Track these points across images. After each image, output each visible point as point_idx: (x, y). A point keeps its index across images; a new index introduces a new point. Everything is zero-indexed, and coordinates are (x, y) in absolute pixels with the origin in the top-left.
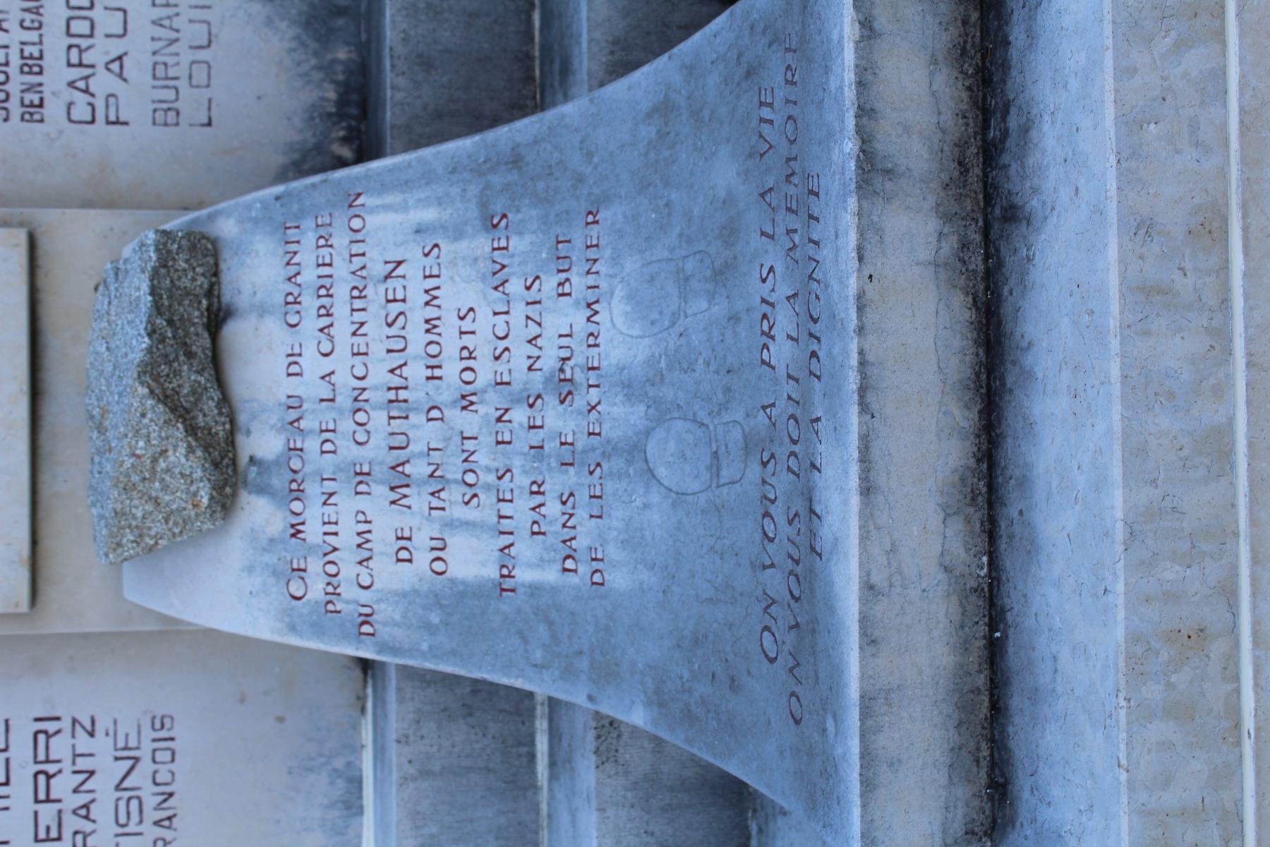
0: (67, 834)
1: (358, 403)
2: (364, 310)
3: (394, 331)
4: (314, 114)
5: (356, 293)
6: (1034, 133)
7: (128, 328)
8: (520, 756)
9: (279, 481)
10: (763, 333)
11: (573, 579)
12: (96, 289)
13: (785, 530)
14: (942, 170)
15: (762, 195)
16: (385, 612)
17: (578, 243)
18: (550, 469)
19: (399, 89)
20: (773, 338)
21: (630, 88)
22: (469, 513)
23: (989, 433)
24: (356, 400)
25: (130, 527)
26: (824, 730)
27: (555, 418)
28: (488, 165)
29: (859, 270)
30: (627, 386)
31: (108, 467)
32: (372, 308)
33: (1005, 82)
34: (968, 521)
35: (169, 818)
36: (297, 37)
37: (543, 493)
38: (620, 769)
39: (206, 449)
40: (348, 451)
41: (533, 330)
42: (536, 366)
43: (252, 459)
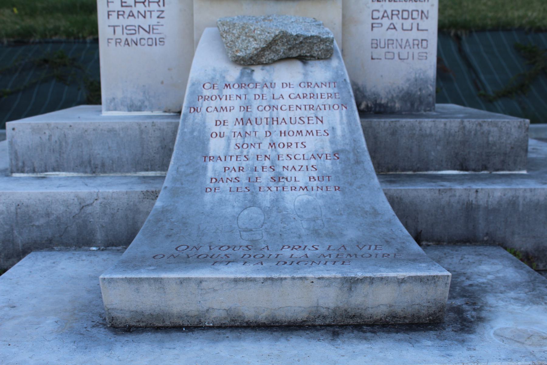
0: (123, 9)
2: (305, 109)
3: (298, 119)
5: (311, 107)
6: (364, 341)
7: (299, 28)
8: (147, 166)
10: (294, 246)
11: (208, 182)
12: (314, 19)
13: (223, 253)
14: (351, 309)
15: (343, 246)
16: (198, 117)
17: (328, 184)
18: (248, 174)
19: (384, 124)
20: (292, 249)
21: (383, 202)
22: (233, 145)
23: (257, 326)
24: (274, 106)
25: (230, 28)
26: (150, 266)
27: (265, 176)
28: (356, 153)
29: (315, 278)
30: (277, 200)
31: (251, 22)
32: (306, 112)
33: (383, 332)
34: (225, 318)
35: (128, 44)
36: (403, 89)
37: (239, 171)
38: (141, 200)
39: (257, 55)
40: (255, 104)
41: (298, 168)
42: (285, 169)
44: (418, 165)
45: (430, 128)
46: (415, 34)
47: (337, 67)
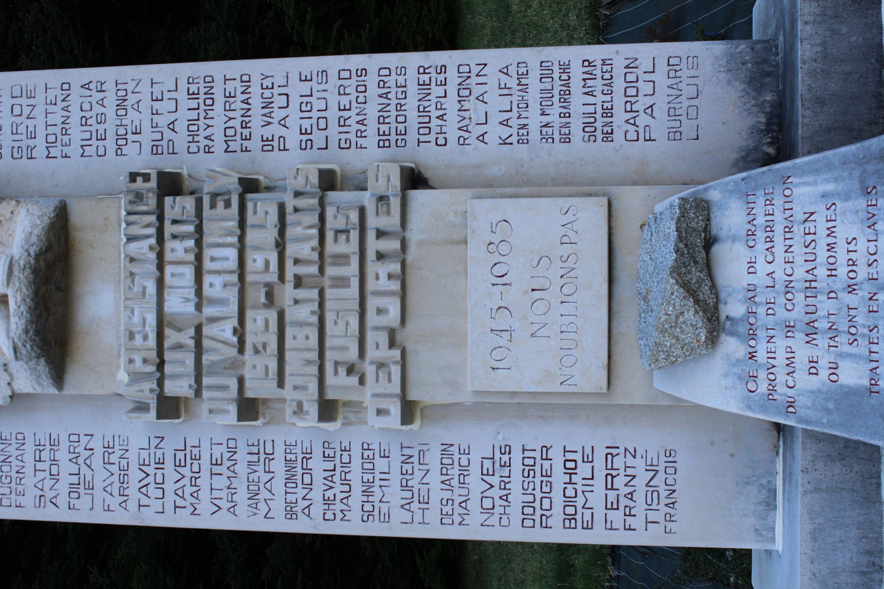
0: (621, 507)
1: (788, 288)
3: (808, 250)
4: (754, 130)
5: (787, 230)
9: (742, 329)
16: (801, 401)
24: (787, 287)
35: (673, 503)
39: (704, 311)
40: (782, 314)
43: (727, 317)
44: (873, 61)
45: (812, 45)
46: (660, 77)
47: (722, 192)
